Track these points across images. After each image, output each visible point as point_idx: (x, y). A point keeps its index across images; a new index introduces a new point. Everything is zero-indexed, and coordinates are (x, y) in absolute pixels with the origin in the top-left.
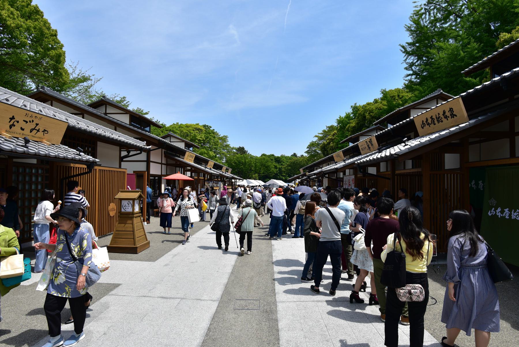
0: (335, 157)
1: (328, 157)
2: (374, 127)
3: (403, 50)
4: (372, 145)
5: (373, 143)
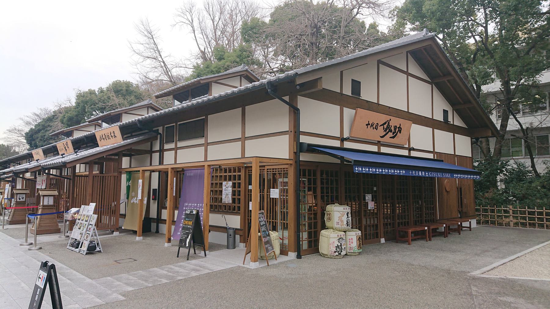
0: (34, 154)
1: (52, 146)
2: (87, 123)
3: (129, 46)
4: (68, 148)
5: (69, 146)
